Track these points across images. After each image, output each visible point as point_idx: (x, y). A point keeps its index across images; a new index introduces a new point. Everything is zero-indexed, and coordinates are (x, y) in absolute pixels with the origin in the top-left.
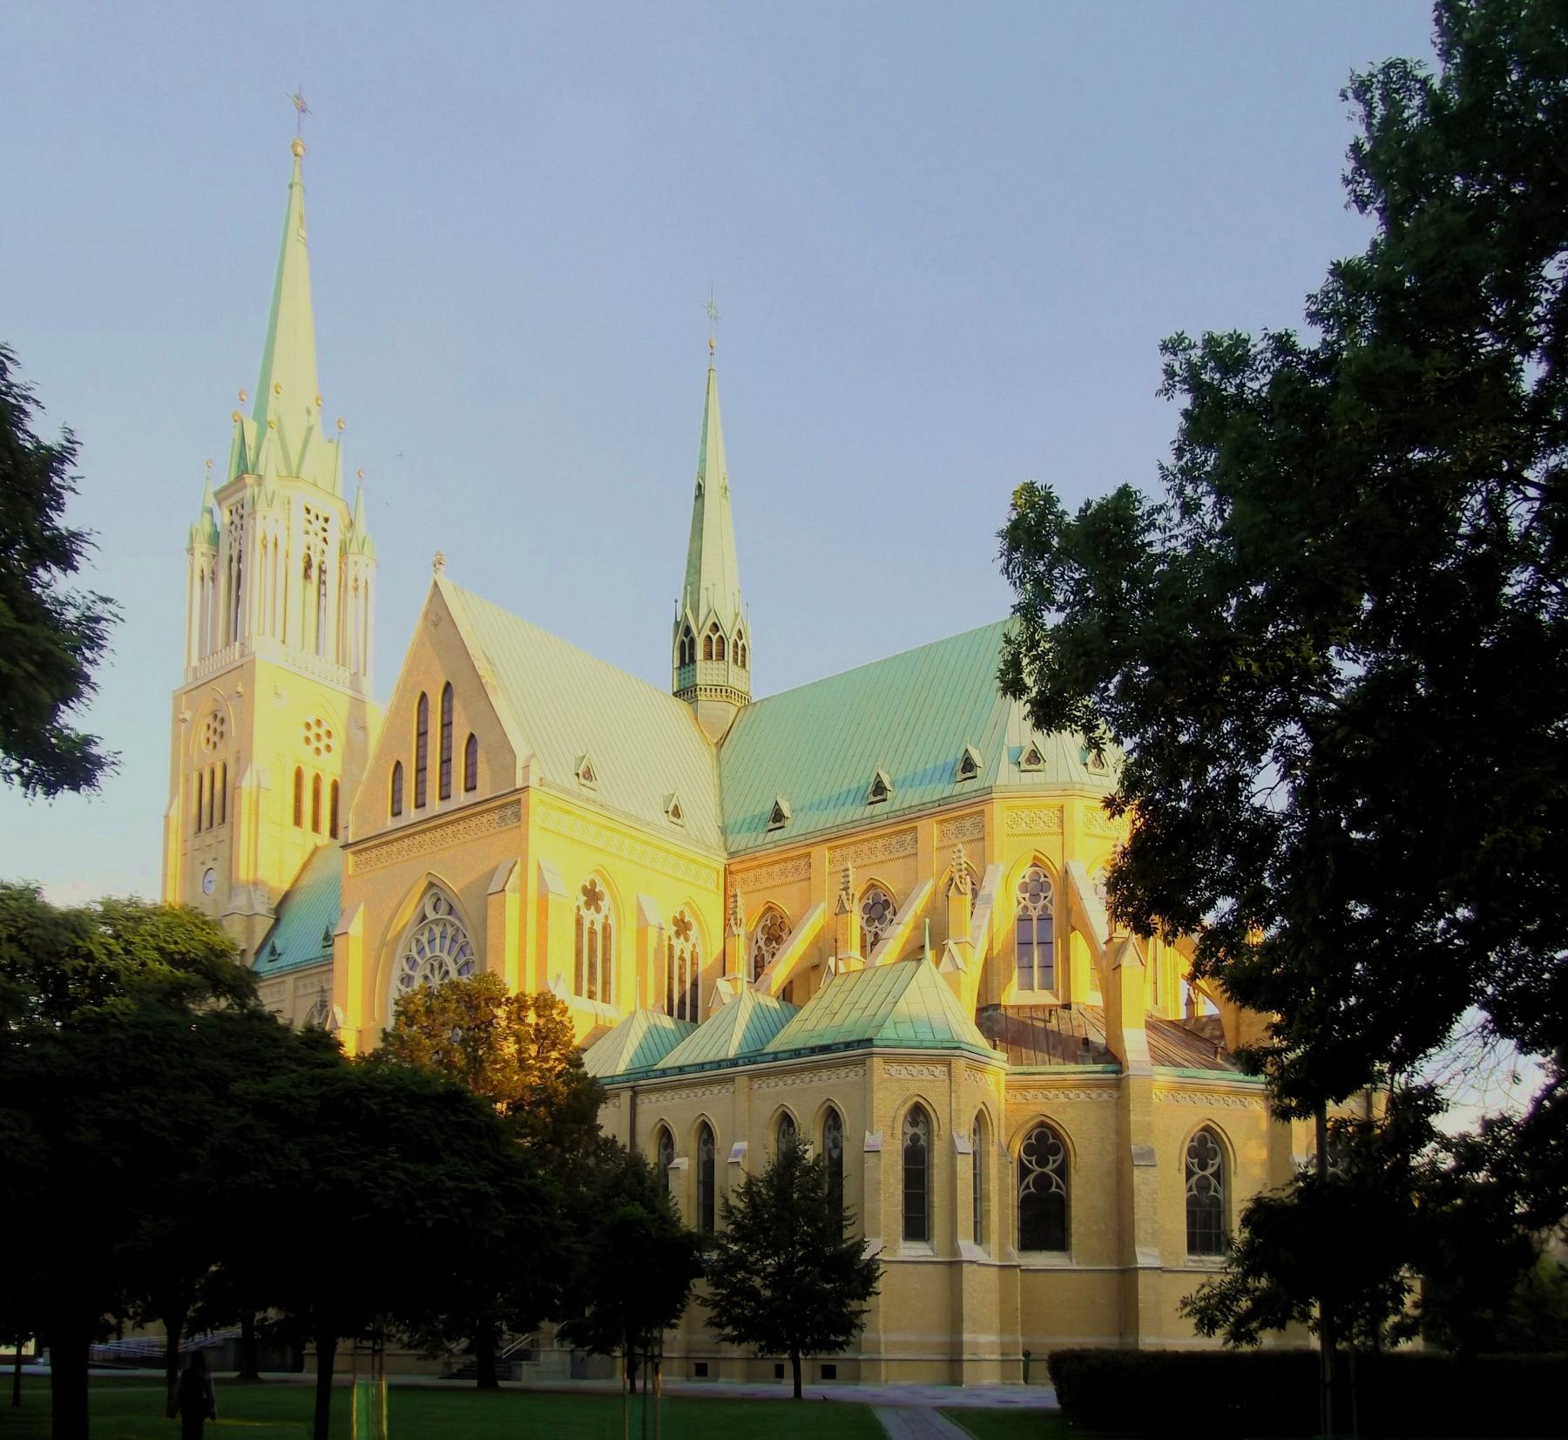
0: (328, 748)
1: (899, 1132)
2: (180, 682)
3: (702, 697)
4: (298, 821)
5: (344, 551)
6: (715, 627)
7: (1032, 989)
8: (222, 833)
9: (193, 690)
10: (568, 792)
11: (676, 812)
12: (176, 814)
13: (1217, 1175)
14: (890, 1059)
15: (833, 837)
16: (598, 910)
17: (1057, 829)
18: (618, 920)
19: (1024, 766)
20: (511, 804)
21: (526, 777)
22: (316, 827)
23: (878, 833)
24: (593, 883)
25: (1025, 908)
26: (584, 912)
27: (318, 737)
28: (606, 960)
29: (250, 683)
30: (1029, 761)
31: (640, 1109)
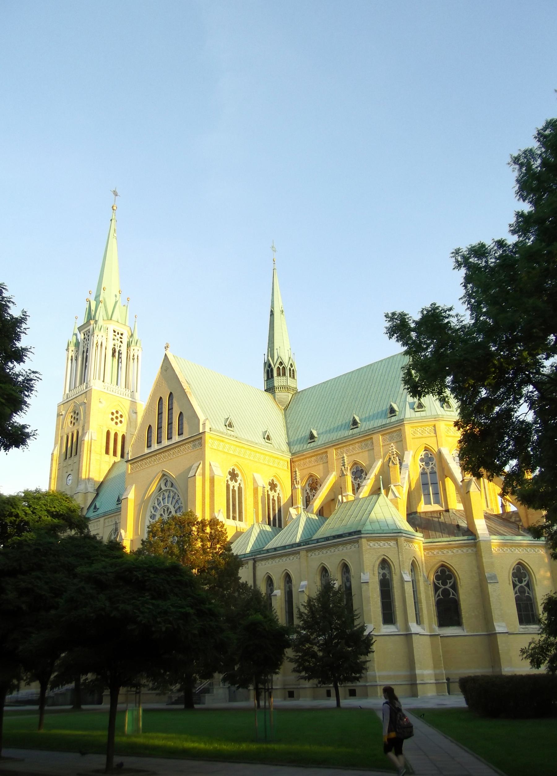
0: (121, 422)
1: (377, 574)
3: (277, 391)
5: (129, 345)
6: (281, 363)
7: (431, 504)
10: (220, 432)
12: (56, 453)
13: (528, 585)
14: (369, 539)
15: (337, 444)
16: (236, 481)
17: (433, 434)
18: (245, 484)
20: (198, 440)
22: (115, 454)
24: (233, 470)
26: (230, 482)
30: (418, 407)
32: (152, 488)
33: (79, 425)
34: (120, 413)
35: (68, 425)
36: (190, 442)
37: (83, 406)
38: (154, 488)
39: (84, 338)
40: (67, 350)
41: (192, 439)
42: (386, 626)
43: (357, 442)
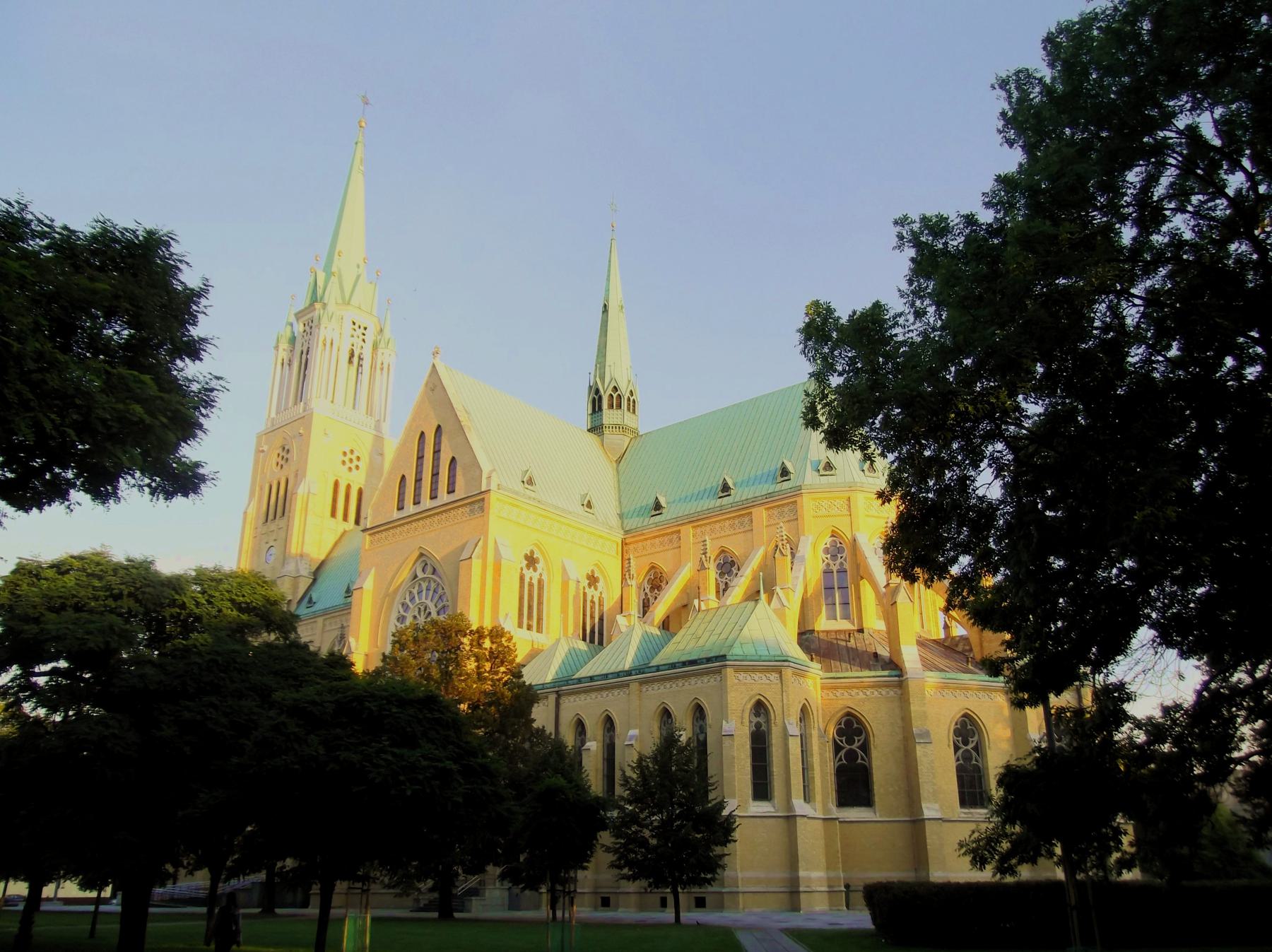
0: (357, 467)
2: (262, 427)
3: (606, 432)
4: (333, 514)
5: (375, 347)
6: (615, 389)
10: (517, 493)
11: (589, 505)
12: (252, 511)
13: (976, 749)
14: (738, 669)
15: (695, 520)
16: (535, 570)
19: (822, 472)
20: (478, 502)
21: (489, 484)
22: (345, 518)
24: (532, 552)
25: (828, 564)
27: (351, 461)
28: (540, 603)
29: (308, 428)
30: (825, 469)
31: (562, 707)
34: (356, 454)
38: (405, 574)
42: (757, 803)
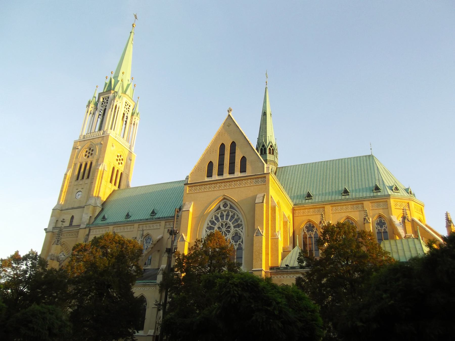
0: (122, 163)
2: (77, 138)
4: (111, 182)
5: (133, 115)
6: (271, 146)
8: (89, 181)
9: (83, 140)
12: (69, 174)
15: (333, 203)
19: (394, 191)
22: (115, 185)
23: (349, 204)
25: (379, 230)
27: (120, 160)
32: (212, 206)
33: (93, 158)
34: (122, 157)
35: (82, 157)
36: (253, 178)
37: (99, 146)
38: (213, 207)
39: (103, 101)
40: (88, 106)
41: (256, 177)
43: (351, 205)
